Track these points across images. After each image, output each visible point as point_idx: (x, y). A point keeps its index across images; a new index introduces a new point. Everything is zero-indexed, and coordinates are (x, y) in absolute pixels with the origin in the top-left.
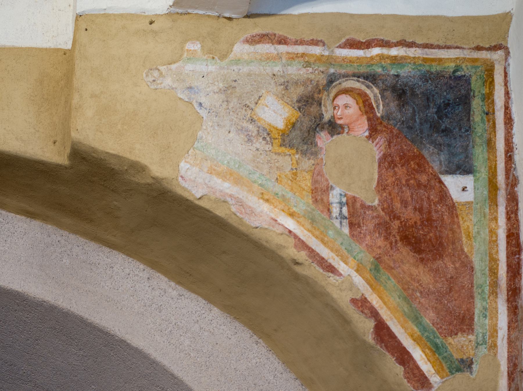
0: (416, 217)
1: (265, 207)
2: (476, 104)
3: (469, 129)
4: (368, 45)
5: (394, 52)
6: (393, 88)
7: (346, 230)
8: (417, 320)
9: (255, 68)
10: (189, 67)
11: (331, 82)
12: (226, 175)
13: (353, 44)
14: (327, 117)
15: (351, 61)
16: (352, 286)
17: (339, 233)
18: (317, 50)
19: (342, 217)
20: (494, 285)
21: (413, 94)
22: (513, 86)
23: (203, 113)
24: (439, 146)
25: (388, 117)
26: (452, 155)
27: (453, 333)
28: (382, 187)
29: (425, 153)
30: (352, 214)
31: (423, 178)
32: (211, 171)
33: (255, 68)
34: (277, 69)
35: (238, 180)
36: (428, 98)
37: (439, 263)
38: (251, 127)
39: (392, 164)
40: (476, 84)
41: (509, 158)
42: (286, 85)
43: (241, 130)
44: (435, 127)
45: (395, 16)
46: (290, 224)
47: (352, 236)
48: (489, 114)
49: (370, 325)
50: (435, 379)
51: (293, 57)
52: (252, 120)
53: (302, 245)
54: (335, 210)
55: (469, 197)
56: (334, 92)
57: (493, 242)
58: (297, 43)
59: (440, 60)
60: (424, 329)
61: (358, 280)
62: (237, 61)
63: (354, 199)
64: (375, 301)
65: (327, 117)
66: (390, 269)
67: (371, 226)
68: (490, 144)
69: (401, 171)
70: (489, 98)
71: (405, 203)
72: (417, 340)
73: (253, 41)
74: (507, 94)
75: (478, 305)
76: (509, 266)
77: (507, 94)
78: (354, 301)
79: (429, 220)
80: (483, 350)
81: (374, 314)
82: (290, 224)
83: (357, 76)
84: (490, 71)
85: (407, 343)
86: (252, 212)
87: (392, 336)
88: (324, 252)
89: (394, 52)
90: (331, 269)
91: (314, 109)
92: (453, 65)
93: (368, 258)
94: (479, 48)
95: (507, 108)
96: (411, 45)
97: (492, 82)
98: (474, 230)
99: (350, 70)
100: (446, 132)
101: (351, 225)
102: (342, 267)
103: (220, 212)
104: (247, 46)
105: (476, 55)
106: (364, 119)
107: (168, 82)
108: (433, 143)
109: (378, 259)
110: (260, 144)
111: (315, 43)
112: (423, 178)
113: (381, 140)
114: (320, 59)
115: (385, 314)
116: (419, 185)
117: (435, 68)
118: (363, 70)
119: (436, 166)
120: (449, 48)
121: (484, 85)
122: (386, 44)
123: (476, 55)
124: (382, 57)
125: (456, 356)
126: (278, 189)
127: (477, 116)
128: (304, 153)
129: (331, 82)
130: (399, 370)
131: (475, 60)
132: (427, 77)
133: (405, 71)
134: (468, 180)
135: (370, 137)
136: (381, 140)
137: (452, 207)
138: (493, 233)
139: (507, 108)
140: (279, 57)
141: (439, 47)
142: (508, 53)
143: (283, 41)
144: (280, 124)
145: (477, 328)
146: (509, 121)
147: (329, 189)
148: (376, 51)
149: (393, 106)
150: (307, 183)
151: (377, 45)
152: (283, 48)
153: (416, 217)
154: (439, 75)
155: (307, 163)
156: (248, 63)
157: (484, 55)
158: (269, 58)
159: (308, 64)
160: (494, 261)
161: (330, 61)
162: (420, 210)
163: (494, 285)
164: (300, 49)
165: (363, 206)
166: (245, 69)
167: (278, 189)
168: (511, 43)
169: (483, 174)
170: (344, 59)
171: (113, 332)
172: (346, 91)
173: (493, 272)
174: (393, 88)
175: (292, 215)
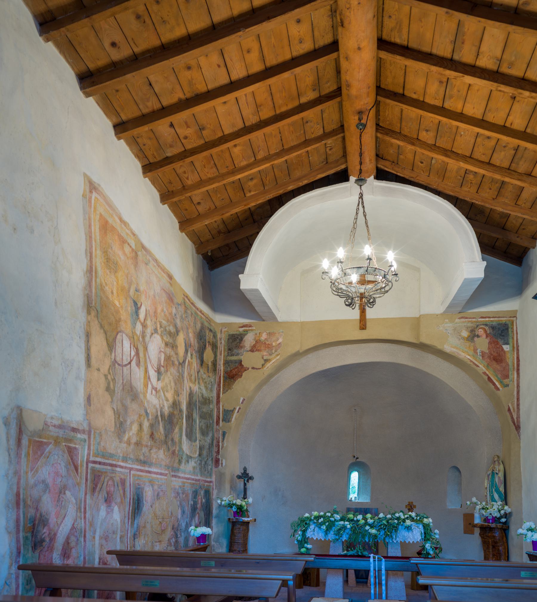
0: (497, 355)
1: (463, 354)
2: (510, 330)
3: (508, 335)
4: (486, 318)
5: (491, 319)
6: (491, 327)
7: (481, 358)
8: (497, 376)
9: (460, 324)
10: (446, 325)
11: (477, 326)
12: (454, 348)
13: (482, 318)
14: (476, 334)
15: (482, 321)
16: (482, 370)
17: (479, 358)
18: (474, 320)
19: (480, 355)
20: (514, 368)
21: (496, 328)
22: (518, 326)
23: (449, 335)
24: (502, 339)
25: (490, 333)
26: (505, 341)
27: (505, 379)
28: (489, 348)
29: (499, 341)
30: (482, 354)
31: (498, 346)
32: (451, 347)
33: (460, 324)
34: (465, 324)
35: (457, 348)
36: (499, 329)
37: (502, 364)
38: (460, 337)
39: (491, 343)
40: (510, 325)
41: (517, 341)
42: (467, 328)
43: (457, 338)
44: (501, 335)
45: (491, 311)
46: (469, 357)
47: (483, 359)
48: (513, 332)
49: (487, 377)
50: (501, 389)
51: (469, 321)
52: (460, 336)
53: (471, 361)
54: (479, 354)
55: (508, 350)
56: (478, 328)
57: (514, 359)
58: (470, 318)
59: (502, 320)
60: (498, 378)
61: (484, 368)
62: (456, 323)
63: (483, 351)
64: (487, 373)
65: (476, 334)
66: (491, 366)
67: (487, 357)
68: (513, 338)
69: (493, 345)
70: (513, 328)
71: (494, 352)
72: (497, 381)
73: (460, 318)
74: (517, 328)
75: (510, 373)
76: (517, 364)
77: (517, 328)
78: (483, 373)
79: (500, 355)
80: (511, 382)
81: (487, 375)
82: (469, 357)
83: (483, 324)
84: (513, 322)
85: (495, 381)
86: (460, 355)
87: (491, 380)
88: (476, 363)
89: (491, 319)
90: (478, 366)
91: (474, 332)
92: (504, 321)
93: (486, 364)
94: (511, 317)
95: (517, 331)
96: (496, 317)
97: (513, 325)
98: (509, 357)
99: (482, 323)
100: (503, 336)
101: (482, 357)
102: (480, 366)
103: (453, 355)
104: (459, 320)
105: (510, 319)
106: (485, 334)
107: (441, 328)
108: (500, 338)
109: (488, 364)
110: (462, 341)
111: (474, 318)
112: (498, 346)
113: (489, 338)
114: (475, 321)
115: (490, 375)
116: (497, 348)
117: (501, 322)
118: (485, 323)
119: (501, 343)
120: (504, 317)
121: (174, 455)
122: (489, 317)
123: (510, 319)
124: (489, 320)
125: (505, 384)
126: (466, 350)
127: (510, 332)
128: (472, 342)
129: (477, 326)
130: (493, 386)
131: (509, 320)
132: (499, 324)
133: (494, 323)
134: (508, 346)
135: (486, 338)
136: (489, 338)
137: (505, 352)
138: (513, 357)
139: (517, 331)
140: (466, 321)
141: (502, 317)
142: (517, 319)
143: (466, 318)
144: (466, 336)
145: (510, 378)
146: (517, 333)
147: (477, 349)
148: (487, 319)
149: (491, 331)
150: (472, 348)
151: (84, 545)
152: (466, 320)
153: (497, 355)
154: (501, 324)
155: (472, 344)
156: (459, 323)
157: (512, 319)
158: (463, 322)
159: (472, 323)
160: (514, 363)
161: (477, 322)
162: (497, 353)
163: (514, 368)
164: (470, 320)
165: (485, 353)
166: (458, 325)
167: (466, 350)
168: (517, 316)
169: (511, 344)
170: (480, 321)
171: (129, 308)
172: (481, 328)
173: (514, 366)
174: (491, 327)
175: (469, 355)
